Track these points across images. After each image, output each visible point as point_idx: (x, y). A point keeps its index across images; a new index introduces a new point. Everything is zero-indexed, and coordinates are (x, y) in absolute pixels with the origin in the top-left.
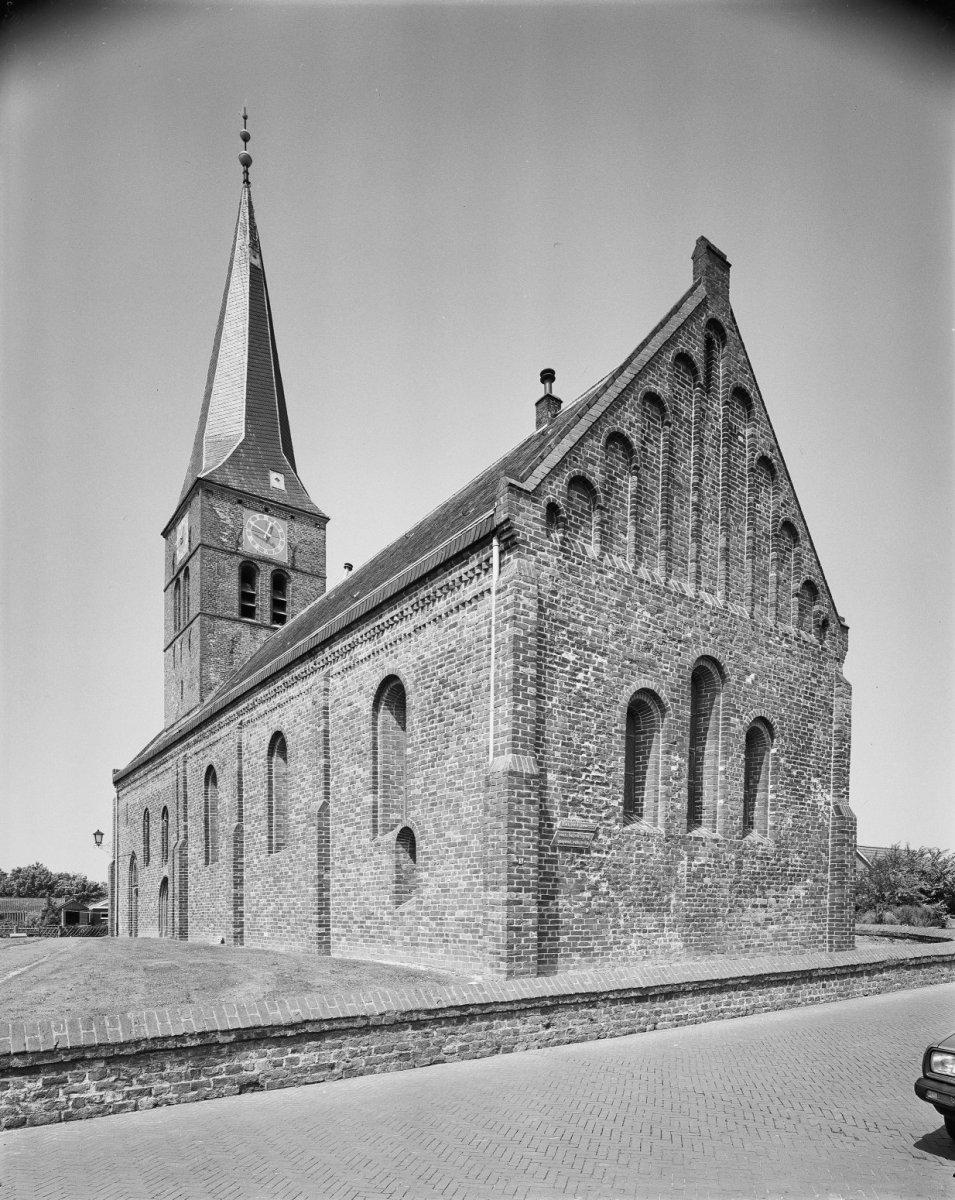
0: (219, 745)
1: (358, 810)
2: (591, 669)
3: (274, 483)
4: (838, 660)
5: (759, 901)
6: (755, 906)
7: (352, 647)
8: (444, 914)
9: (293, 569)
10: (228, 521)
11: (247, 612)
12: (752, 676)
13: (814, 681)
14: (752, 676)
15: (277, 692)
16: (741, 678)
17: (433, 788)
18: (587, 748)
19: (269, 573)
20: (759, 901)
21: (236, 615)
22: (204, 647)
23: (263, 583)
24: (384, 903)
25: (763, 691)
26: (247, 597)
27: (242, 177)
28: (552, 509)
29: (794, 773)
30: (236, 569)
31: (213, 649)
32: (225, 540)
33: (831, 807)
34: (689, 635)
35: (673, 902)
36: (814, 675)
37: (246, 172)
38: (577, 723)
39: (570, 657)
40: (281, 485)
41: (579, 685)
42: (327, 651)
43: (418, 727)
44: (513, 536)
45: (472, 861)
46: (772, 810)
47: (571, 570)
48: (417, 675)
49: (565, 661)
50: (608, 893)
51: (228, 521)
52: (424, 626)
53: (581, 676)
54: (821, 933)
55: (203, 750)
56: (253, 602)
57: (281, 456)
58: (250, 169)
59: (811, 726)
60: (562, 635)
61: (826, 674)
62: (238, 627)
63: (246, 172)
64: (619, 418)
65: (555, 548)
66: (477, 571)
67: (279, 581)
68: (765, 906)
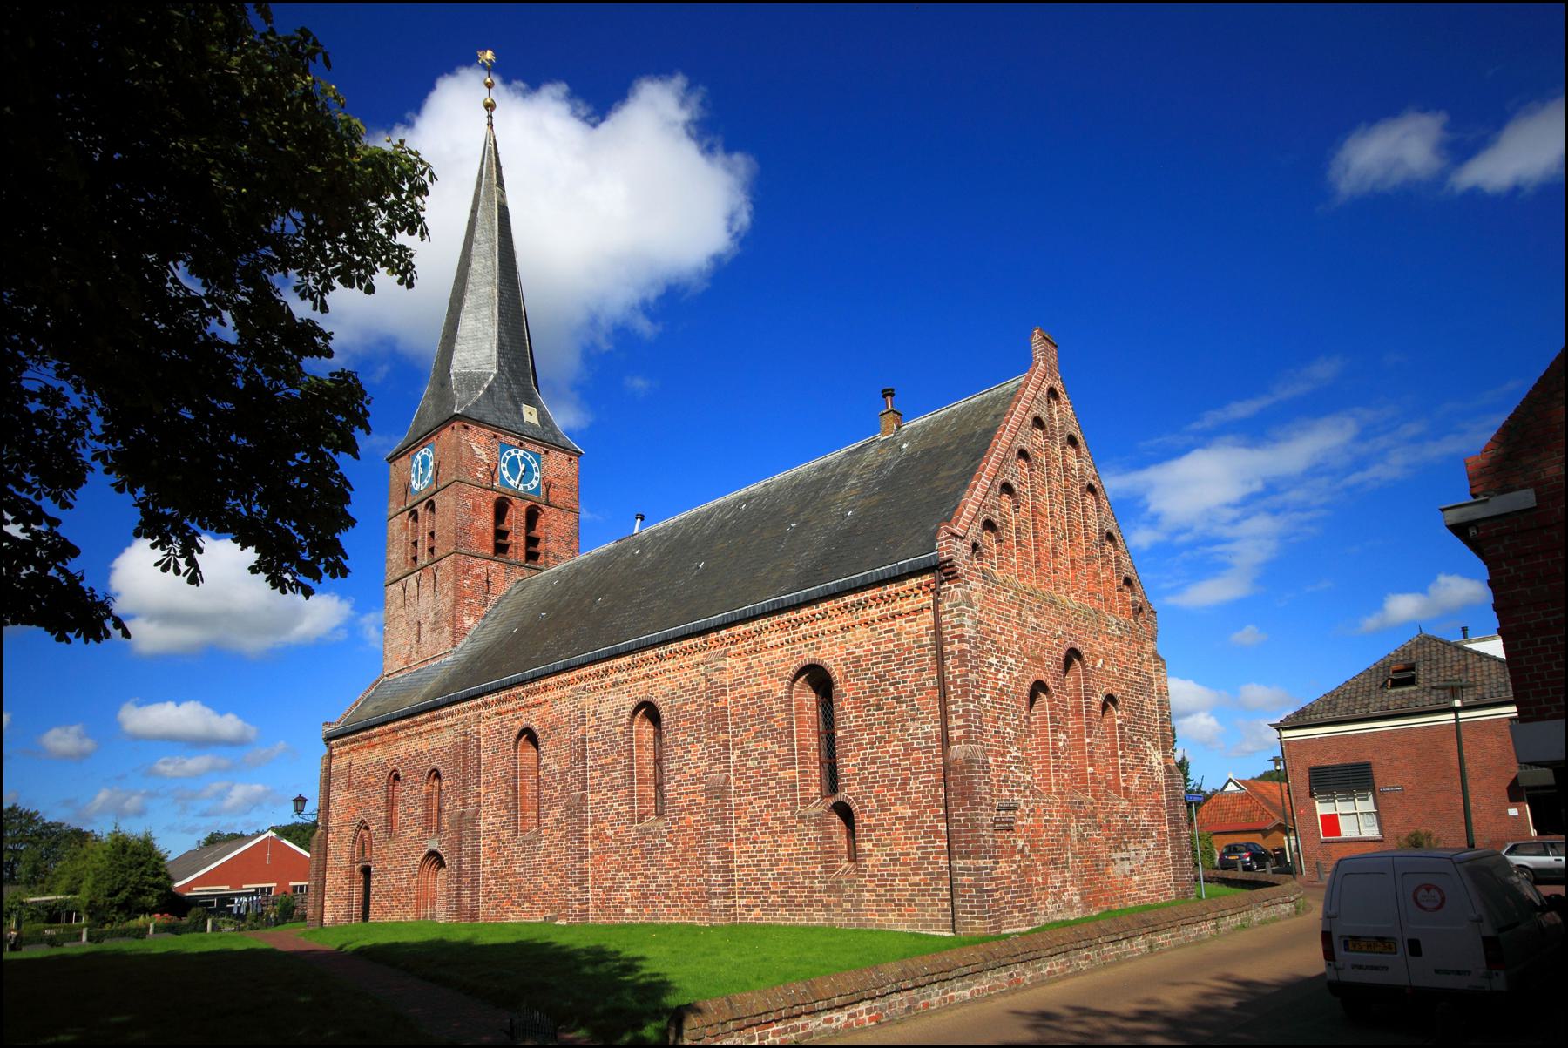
0: (542, 709)
1: (773, 783)
2: (1006, 669)
3: (526, 417)
4: (1152, 640)
5: (1125, 855)
6: (1122, 859)
7: (759, 632)
8: (894, 881)
9: (548, 504)
10: (484, 457)
11: (501, 549)
12: (1101, 661)
13: (1139, 659)
14: (1101, 661)
15: (647, 661)
16: (1095, 662)
17: (874, 768)
18: (1009, 733)
19: (524, 508)
20: (1125, 855)
21: (490, 552)
22: (457, 589)
23: (516, 519)
24: (814, 873)
25: (1108, 672)
26: (500, 534)
27: (486, 121)
28: (975, 546)
29: (1135, 739)
30: (491, 505)
31: (467, 590)
32: (481, 476)
33: (1162, 767)
34: (1060, 633)
35: (1070, 860)
36: (1139, 655)
37: (490, 116)
38: (1001, 713)
39: (994, 660)
40: (534, 420)
41: (1001, 683)
42: (723, 633)
43: (851, 713)
44: (955, 572)
45: (925, 832)
46: (1123, 773)
47: (990, 591)
48: (847, 668)
49: (991, 664)
50: (1030, 856)
51: (484, 457)
52: (854, 626)
53: (1000, 675)
54: (1168, 881)
55: (513, 710)
56: (505, 538)
57: (532, 390)
58: (494, 114)
59: (1141, 698)
60: (988, 645)
61: (1146, 653)
62: (493, 565)
63: (490, 116)
64: (1006, 472)
65: (979, 577)
66: (916, 591)
67: (532, 516)
68: (1128, 859)
